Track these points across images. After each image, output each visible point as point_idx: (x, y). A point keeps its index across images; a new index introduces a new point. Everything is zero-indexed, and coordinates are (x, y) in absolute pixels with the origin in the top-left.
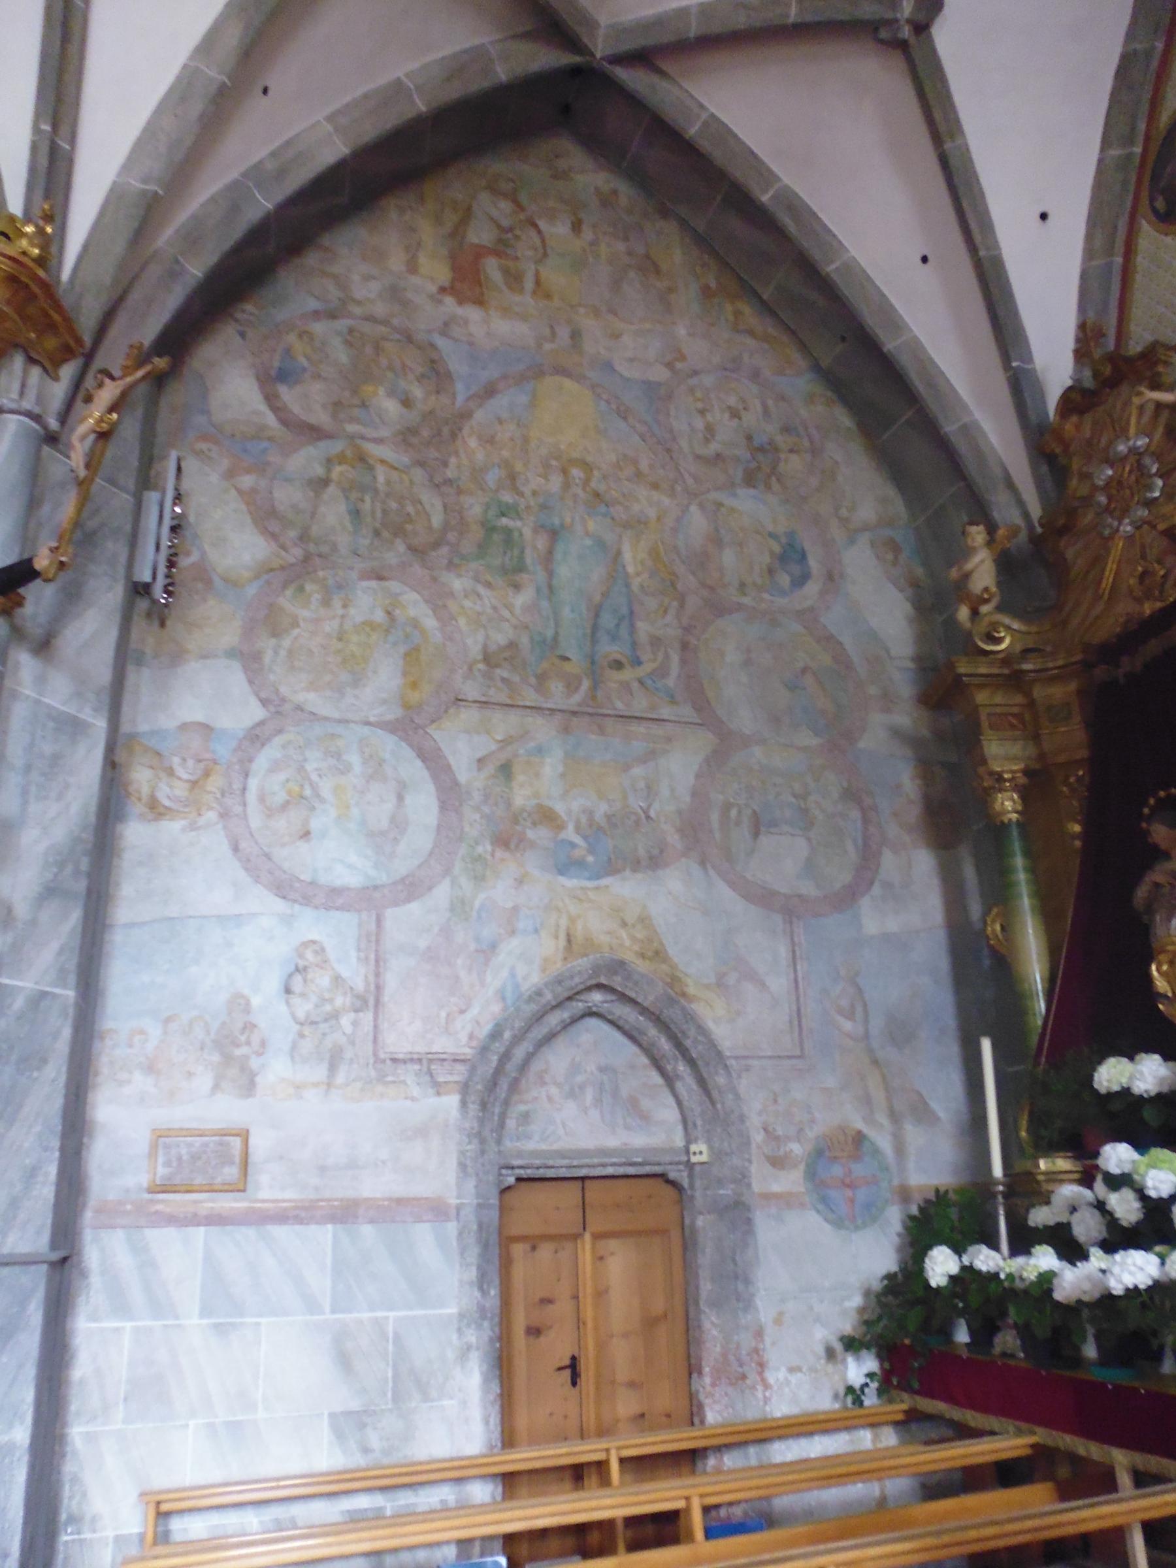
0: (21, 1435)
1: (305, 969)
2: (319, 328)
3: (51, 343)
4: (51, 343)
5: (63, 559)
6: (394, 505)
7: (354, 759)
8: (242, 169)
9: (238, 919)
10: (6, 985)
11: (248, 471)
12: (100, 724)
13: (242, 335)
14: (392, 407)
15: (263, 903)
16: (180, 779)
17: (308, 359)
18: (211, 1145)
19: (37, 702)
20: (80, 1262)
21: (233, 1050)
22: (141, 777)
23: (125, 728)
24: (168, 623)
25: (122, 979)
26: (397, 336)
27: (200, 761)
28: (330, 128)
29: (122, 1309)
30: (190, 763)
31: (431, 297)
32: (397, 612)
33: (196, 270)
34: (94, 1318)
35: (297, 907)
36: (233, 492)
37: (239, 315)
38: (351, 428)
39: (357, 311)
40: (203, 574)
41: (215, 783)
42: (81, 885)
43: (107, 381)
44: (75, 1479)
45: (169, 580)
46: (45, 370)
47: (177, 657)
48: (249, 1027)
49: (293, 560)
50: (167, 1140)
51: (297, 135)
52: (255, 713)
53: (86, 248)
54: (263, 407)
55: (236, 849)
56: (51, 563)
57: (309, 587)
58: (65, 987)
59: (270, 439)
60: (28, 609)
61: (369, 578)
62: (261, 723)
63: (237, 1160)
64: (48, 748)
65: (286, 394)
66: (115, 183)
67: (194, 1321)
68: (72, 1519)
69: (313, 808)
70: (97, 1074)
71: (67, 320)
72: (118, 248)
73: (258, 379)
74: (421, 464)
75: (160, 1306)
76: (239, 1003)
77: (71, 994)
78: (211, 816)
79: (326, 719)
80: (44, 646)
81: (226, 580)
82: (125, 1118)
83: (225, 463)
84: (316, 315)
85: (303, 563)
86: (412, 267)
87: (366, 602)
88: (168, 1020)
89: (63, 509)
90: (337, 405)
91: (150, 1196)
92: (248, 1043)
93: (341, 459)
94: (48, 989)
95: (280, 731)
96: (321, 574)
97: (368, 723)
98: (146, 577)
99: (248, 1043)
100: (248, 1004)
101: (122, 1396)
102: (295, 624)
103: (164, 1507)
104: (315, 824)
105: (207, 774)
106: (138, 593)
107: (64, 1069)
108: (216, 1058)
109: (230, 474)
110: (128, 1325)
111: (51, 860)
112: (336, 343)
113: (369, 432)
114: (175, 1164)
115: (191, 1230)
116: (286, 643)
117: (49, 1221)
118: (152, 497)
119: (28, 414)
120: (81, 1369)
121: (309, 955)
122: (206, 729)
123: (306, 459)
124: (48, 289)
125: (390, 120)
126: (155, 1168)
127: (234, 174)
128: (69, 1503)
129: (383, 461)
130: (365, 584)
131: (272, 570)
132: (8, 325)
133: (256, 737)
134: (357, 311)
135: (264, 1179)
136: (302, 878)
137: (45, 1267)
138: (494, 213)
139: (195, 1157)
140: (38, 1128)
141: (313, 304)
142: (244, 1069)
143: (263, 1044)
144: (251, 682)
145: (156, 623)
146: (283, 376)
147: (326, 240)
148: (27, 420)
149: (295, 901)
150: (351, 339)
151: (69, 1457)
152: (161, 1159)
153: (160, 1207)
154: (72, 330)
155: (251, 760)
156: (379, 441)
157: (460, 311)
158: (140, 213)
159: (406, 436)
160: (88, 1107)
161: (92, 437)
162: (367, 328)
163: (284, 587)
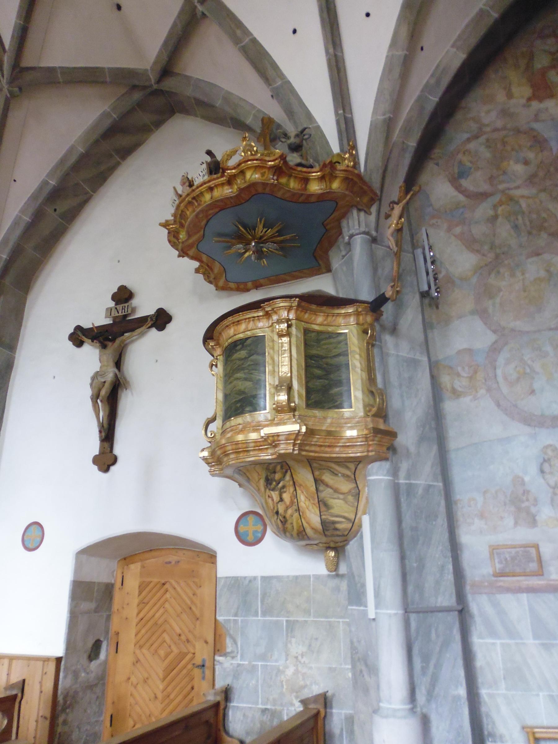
0: (462, 691)
1: (549, 459)
2: (472, 146)
3: (365, 200)
4: (365, 200)
5: (398, 289)
6: (534, 216)
7: (549, 348)
8: (420, 88)
9: (508, 440)
10: (414, 484)
11: (457, 226)
12: (425, 359)
13: (437, 164)
14: (519, 168)
15: (518, 430)
16: (463, 377)
17: (471, 162)
18: (521, 552)
19: (398, 356)
20: (468, 611)
21: (521, 505)
22: (445, 380)
23: (433, 359)
24: (440, 306)
25: (460, 476)
26: (511, 133)
27: (471, 367)
28: (455, 50)
29: (493, 634)
30: (466, 368)
31: (524, 106)
32: (552, 269)
33: (413, 143)
34: (481, 637)
35: (537, 429)
36: (453, 237)
37: (433, 156)
38: (501, 187)
39: (488, 129)
40: (450, 280)
41: (480, 376)
42: (434, 434)
43: (395, 206)
44: (488, 715)
45: (436, 287)
46: (365, 212)
47: (448, 321)
48: (526, 492)
49: (490, 260)
50: (498, 551)
51: (440, 62)
52: (491, 338)
53: (367, 154)
54: (456, 193)
55: (498, 405)
56: (393, 293)
57: (502, 270)
58: (438, 482)
59: (464, 207)
60: (384, 317)
61: (532, 256)
62: (496, 342)
63: (535, 559)
64: (406, 375)
65: (465, 183)
66: (371, 122)
67: (530, 641)
68: (490, 735)
69: (533, 378)
70: (457, 521)
71: (369, 187)
72: (381, 148)
73: (450, 181)
74: (544, 190)
75: (512, 633)
76: (518, 481)
77: (441, 484)
78: (482, 392)
79: (528, 332)
80: (394, 330)
81: (461, 279)
82: (476, 541)
83: (445, 226)
84: (469, 140)
85: (496, 259)
86: (510, 95)
87: (533, 269)
88: (485, 493)
89: (389, 267)
90: (491, 179)
91: (495, 579)
92: (527, 500)
93: (501, 203)
94: (431, 483)
95: (506, 344)
96: (506, 262)
97: (551, 329)
98: (426, 288)
99: (527, 500)
100: (523, 480)
101: (502, 677)
102: (500, 290)
103: (538, 735)
104: (537, 385)
105: (476, 372)
106: (425, 297)
107: (445, 520)
108: (513, 509)
109: (449, 230)
110: (498, 642)
111: (419, 424)
112: (482, 149)
113: (512, 185)
114: (504, 562)
115: (520, 595)
116: (498, 300)
117: (454, 591)
118: (419, 251)
119: (364, 233)
120: (480, 662)
121: (550, 453)
122: (470, 351)
123: (484, 210)
124: (359, 176)
125: (482, 30)
126: (495, 564)
127: (418, 93)
128: (487, 728)
129: (523, 197)
130: (530, 260)
131: (481, 267)
132: (347, 199)
133: (494, 350)
134: (488, 129)
135: (552, 569)
136: (536, 413)
137: (456, 613)
138: (547, 48)
139: (513, 559)
140: (440, 548)
141: (466, 136)
142: (528, 512)
143: (536, 500)
144: (486, 324)
145: (435, 308)
146: (463, 174)
147: (463, 104)
148: (364, 236)
149: (535, 426)
150: (489, 144)
151: (482, 704)
152: (496, 561)
153: (501, 584)
154: (372, 191)
155: (495, 361)
156: (518, 187)
157: (542, 106)
158: (385, 127)
159: (531, 179)
160: (457, 537)
161: (396, 233)
162: (496, 135)
163: (490, 274)
